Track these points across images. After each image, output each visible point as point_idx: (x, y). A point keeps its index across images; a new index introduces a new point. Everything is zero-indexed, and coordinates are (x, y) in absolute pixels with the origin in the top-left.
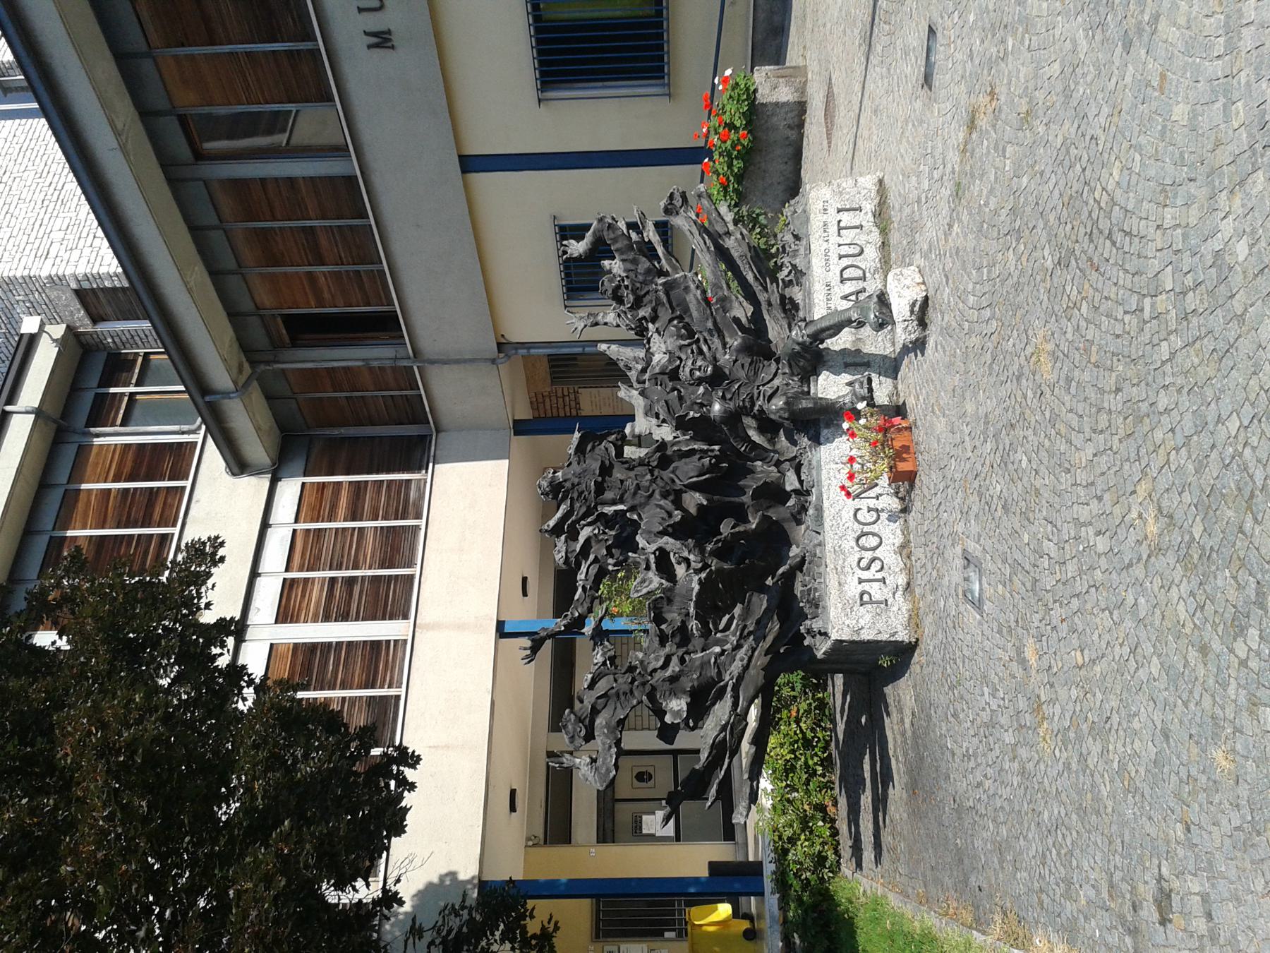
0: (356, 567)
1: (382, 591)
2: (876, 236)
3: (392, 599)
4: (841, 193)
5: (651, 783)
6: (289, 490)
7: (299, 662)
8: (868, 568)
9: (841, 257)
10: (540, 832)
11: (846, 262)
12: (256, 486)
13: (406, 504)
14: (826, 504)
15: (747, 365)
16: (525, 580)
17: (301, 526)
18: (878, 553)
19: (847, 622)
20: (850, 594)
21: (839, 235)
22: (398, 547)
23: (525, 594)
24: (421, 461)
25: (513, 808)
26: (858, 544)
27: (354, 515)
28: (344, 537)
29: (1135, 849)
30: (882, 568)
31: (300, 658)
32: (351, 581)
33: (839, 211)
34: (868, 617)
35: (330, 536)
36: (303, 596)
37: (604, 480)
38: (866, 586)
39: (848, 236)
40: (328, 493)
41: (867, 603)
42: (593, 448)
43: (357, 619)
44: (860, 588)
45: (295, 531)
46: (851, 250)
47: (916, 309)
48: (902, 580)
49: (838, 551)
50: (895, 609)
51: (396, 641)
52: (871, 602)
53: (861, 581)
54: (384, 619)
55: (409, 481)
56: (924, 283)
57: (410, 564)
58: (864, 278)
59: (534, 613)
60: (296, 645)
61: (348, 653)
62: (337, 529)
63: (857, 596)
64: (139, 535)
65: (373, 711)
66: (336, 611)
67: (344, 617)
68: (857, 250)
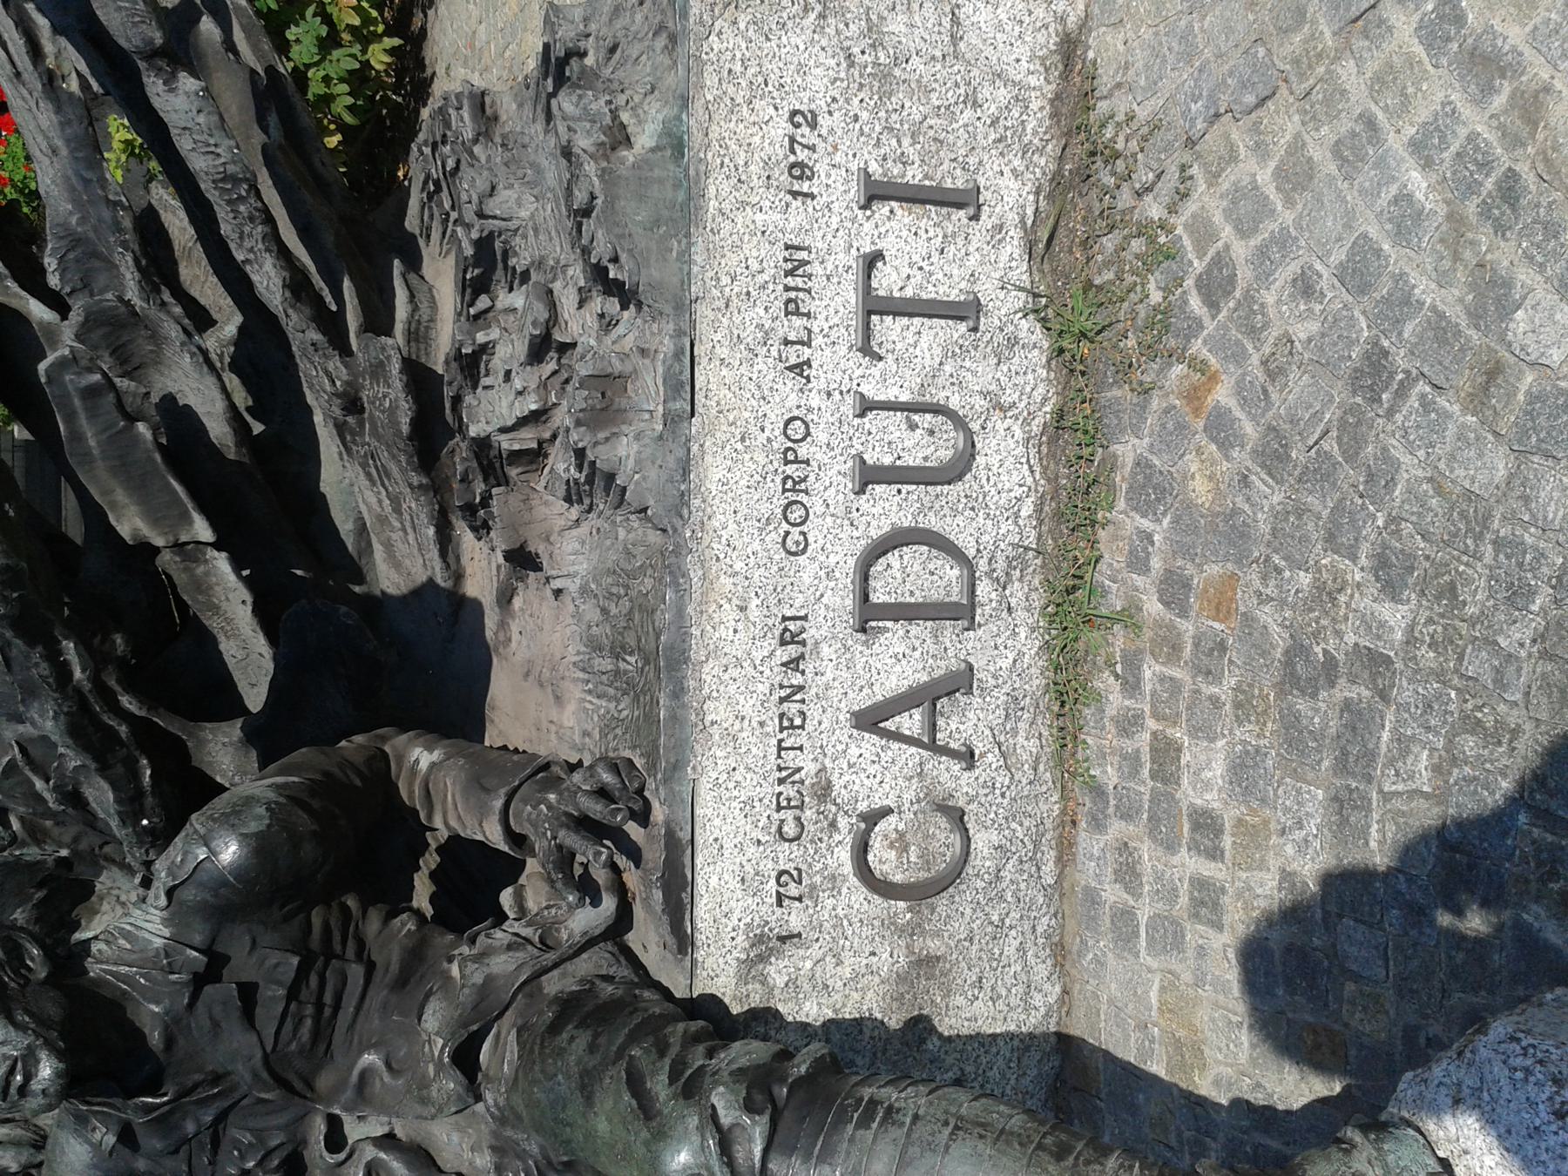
2: (1030, 379)
4: (884, 80)
9: (868, 476)
11: (888, 509)
15: (273, 995)
33: (875, 193)
44: (786, 295)
46: (919, 445)
53: (787, 289)
58: (962, 613)
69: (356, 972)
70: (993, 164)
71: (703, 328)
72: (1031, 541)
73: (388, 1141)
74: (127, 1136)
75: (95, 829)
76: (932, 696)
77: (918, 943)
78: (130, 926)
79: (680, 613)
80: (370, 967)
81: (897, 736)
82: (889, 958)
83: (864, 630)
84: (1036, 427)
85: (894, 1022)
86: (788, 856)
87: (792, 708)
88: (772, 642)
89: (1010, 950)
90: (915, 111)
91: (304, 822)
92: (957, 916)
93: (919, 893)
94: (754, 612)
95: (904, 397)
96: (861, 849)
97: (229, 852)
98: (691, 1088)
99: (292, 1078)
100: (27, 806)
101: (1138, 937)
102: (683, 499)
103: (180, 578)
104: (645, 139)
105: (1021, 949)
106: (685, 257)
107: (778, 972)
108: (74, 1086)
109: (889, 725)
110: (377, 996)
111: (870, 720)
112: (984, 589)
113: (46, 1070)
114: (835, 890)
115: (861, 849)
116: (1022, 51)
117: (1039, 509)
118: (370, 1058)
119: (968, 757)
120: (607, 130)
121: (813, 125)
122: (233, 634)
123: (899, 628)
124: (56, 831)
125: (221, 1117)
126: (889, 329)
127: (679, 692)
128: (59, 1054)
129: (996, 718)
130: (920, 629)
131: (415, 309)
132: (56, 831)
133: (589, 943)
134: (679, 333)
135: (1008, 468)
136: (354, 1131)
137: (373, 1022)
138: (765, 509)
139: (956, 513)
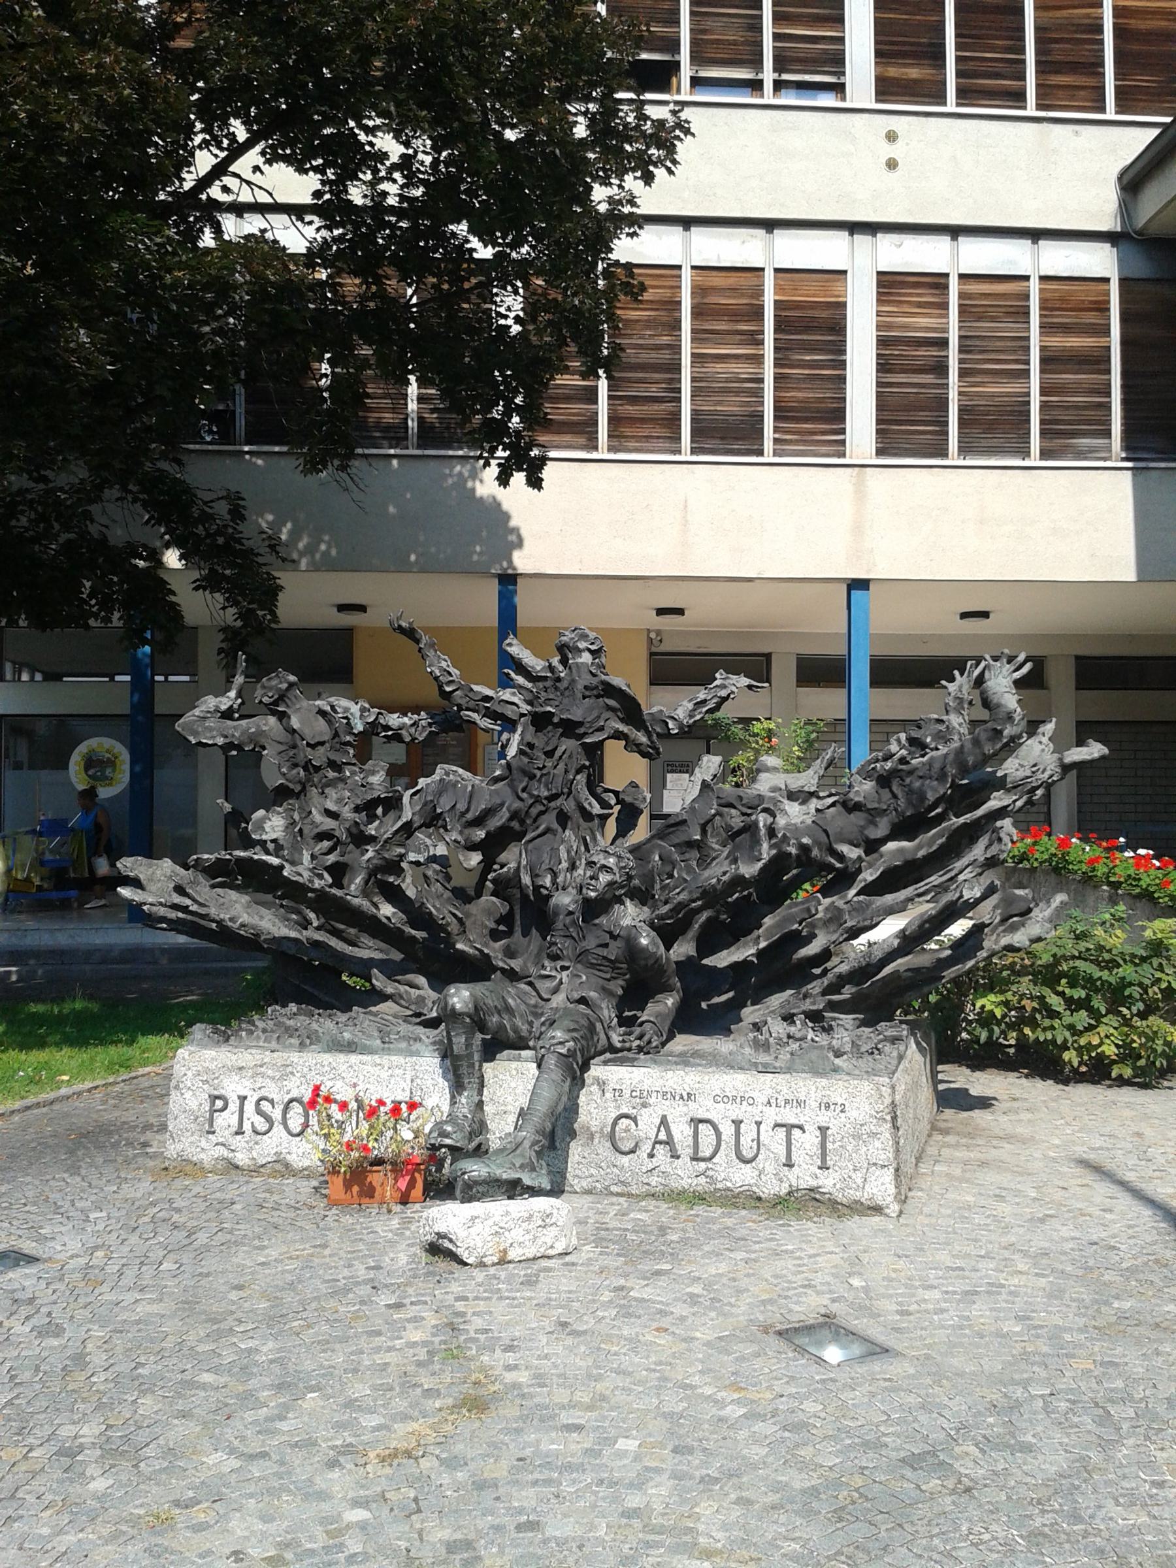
0: (963, 373)
1: (923, 415)
2: (771, 1187)
3: (910, 427)
6: (1100, 261)
8: (260, 1112)
9: (737, 1123)
10: (665, 647)
11: (727, 1131)
12: (1103, 211)
13: (1069, 433)
14: (354, 1058)
16: (985, 615)
17: (1034, 287)
18: (278, 1129)
19: (189, 1074)
20: (225, 1081)
21: (777, 1125)
22: (995, 430)
23: (964, 615)
24: (1144, 449)
25: (661, 612)
26: (291, 1101)
27: (1049, 361)
28: (1014, 351)
29: (770, 1388)
30: (258, 1133)
31: (824, 314)
32: (941, 368)
33: (823, 1130)
34: (193, 1104)
35: (1018, 330)
36: (920, 305)
37: (556, 726)
38: (234, 1106)
39: (775, 1142)
40: (1091, 318)
41: (213, 1104)
42: (609, 708)
45: (1026, 278)
46: (747, 1141)
47: (447, 1244)
48: (241, 1158)
49: (286, 1072)
50: (203, 1144)
51: (843, 442)
52: (213, 1111)
54: (879, 422)
55: (1108, 434)
56: (503, 1261)
57: (965, 449)
59: (888, 626)
60: (844, 305)
62: (1028, 338)
63: (223, 1092)
64: (1023, 62)
67: (884, 366)
68: (747, 1153)
69: (608, 976)
70: (837, 1176)
71: (783, 1076)
72: (719, 1186)
73: (561, 983)
74: (571, 913)
76: (669, 1142)
77: (598, 1135)
78: (630, 915)
79: (700, 1065)
80: (609, 980)
81: (659, 1131)
82: (595, 1125)
83: (692, 1120)
84: (754, 1189)
85: (576, 1126)
86: (626, 1093)
87: (669, 1096)
88: (688, 1090)
89: (593, 1171)
90: (849, 1148)
91: (651, 962)
92: (603, 1149)
93: (612, 1137)
94: (697, 1086)
95: (761, 1138)
96: (626, 1116)
97: (644, 941)
98: (574, 1039)
99: (581, 957)
102: (732, 1068)
103: (749, 938)
104: (837, 1061)
105: (592, 1176)
106: (803, 1071)
107: (595, 1088)
108: (587, 901)
109: (662, 1128)
110: (601, 981)
111: (664, 1121)
112: (703, 1165)
113: (593, 894)
114: (615, 1107)
115: (626, 1116)
116: (875, 1191)
117: (728, 1189)
118: (584, 978)
119: (651, 1156)
120: (838, 1050)
121: (842, 1111)
122: (729, 955)
123: (691, 1133)
125: (573, 938)
126: (782, 1133)
127: (676, 1063)
129: (662, 1168)
130: (690, 1140)
133: (608, 1038)
134: (781, 1068)
135: (741, 1177)
136: (565, 974)
137: (594, 980)
138: (727, 1090)
139: (726, 1156)
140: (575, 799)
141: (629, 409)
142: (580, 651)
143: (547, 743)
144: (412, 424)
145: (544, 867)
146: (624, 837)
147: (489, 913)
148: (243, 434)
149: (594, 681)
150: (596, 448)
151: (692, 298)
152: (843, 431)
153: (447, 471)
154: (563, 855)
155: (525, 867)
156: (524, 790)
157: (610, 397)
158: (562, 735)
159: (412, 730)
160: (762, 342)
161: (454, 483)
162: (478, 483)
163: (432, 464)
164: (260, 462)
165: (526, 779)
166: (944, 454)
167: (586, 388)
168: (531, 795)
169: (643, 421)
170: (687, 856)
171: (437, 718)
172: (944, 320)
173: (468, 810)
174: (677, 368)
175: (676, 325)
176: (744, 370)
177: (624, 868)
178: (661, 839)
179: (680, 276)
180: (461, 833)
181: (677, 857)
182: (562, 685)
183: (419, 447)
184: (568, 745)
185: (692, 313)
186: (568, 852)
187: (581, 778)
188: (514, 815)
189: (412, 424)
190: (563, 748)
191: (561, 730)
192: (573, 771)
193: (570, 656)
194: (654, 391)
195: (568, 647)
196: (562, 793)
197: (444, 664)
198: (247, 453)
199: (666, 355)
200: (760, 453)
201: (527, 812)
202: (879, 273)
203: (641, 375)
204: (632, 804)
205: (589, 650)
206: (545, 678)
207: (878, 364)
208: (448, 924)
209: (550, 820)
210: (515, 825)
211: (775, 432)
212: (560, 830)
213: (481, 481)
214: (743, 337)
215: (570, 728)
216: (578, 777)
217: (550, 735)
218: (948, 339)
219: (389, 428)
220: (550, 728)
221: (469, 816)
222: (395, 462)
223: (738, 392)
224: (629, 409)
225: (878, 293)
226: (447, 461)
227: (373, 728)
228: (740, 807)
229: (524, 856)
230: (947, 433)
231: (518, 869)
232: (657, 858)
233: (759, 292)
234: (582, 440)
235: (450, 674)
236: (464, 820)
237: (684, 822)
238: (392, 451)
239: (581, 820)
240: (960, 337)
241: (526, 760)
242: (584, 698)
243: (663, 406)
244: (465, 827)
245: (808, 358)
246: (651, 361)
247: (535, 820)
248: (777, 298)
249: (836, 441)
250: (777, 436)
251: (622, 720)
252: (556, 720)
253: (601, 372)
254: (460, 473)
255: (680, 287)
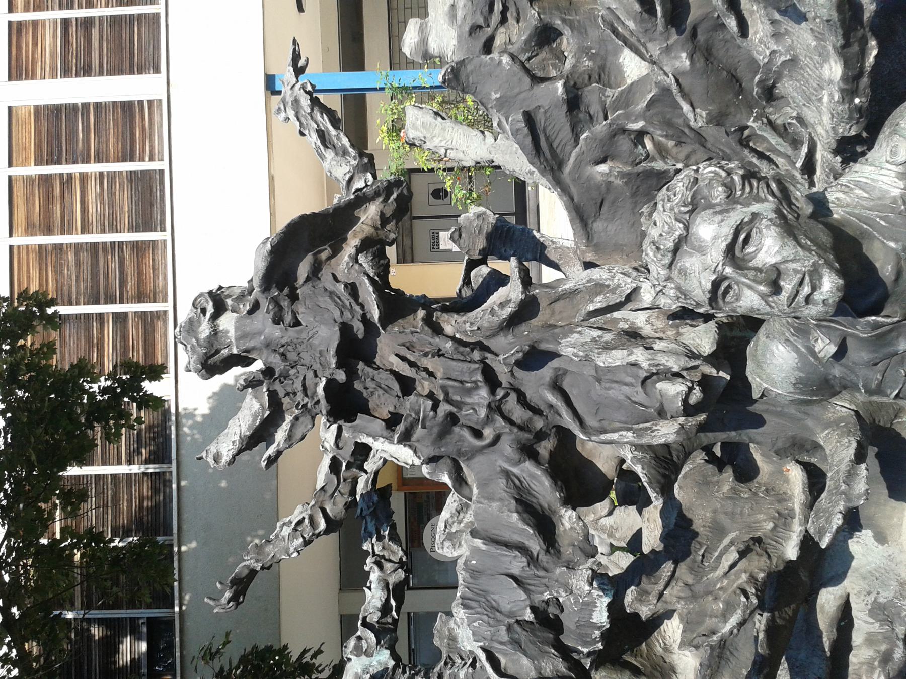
5: (447, 200)
7: (44, 130)
31: (44, 123)
32: (87, 23)
36: (35, 44)
37: (352, 374)
42: (315, 272)
43: (101, 74)
51: (150, 102)
54: (132, 72)
60: (37, 108)
61: (97, 116)
65: (137, 189)
66: (76, 65)
67: (86, 71)
75: (705, 147)
100: (662, 130)
101: (61, 529)
124: (675, 151)
128: (842, 272)
131: (57, 125)
132: (675, 151)
140: (493, 336)
141: (131, 284)
142: (215, 333)
143: (387, 390)
144: (152, 469)
145: (640, 397)
146: (543, 247)
147: (705, 484)
148: (165, 610)
149: (264, 304)
150: (165, 312)
151: (36, 235)
152: (141, 102)
153: (189, 438)
154: (617, 358)
155: (639, 433)
156: (478, 434)
157: (121, 302)
158: (370, 362)
159: (388, 566)
160: (70, 175)
161: (199, 433)
162: (197, 413)
163: (183, 452)
164: (187, 597)
165: (456, 429)
166: (156, 16)
167: (114, 323)
168: (488, 420)
169: (140, 273)
170: (595, 109)
171: (371, 527)
172: (47, 23)
173: (523, 549)
174: (94, 246)
175: (58, 248)
176: (93, 190)
177: (730, 188)
178: (560, 165)
179: (19, 247)
180: (571, 566)
181: (601, 127)
182: (276, 361)
183: (170, 462)
184: (387, 350)
185: (48, 234)
186: (608, 347)
187: (451, 324)
188: (528, 452)
189: (152, 469)
190: (394, 360)
191: (361, 365)
192: (437, 340)
193: (225, 352)
194: (114, 265)
195: (208, 357)
196: (482, 361)
197: (286, 531)
198: (180, 608)
199: (84, 256)
200: (161, 172)
201: (521, 428)
202: (10, 79)
203: (102, 276)
204: (490, 237)
205: (216, 316)
206: (273, 395)
207: (84, 76)
208: (752, 579)
209: (536, 385)
210: (545, 448)
211: (144, 161)
212: (554, 363)
213: (195, 410)
214: (66, 191)
215: (355, 349)
216: (449, 329)
217: (371, 385)
218: (62, 19)
219: (155, 491)
220: (358, 386)
221: (535, 545)
222: (183, 483)
223: (112, 194)
224: (131, 284)
225: (26, 79)
226: (181, 438)
227: (384, 632)
228: (489, 31)
229: (615, 436)
230: (140, 15)
231: (638, 447)
232: (603, 168)
233: (29, 180)
234: (159, 324)
235: (300, 522)
236: (543, 558)
237: (529, 119)
238: (174, 486)
239: (535, 322)
240: (60, 8)
241: (419, 432)
242: (297, 323)
243: (127, 256)
244: (558, 552)
245: (81, 135)
246: (89, 268)
247: (537, 411)
248: (33, 164)
249: (149, 108)
250: (147, 159)
251: (336, 250)
252: (341, 376)
253: (50, 311)
254: (190, 427)
255: (27, 246)
